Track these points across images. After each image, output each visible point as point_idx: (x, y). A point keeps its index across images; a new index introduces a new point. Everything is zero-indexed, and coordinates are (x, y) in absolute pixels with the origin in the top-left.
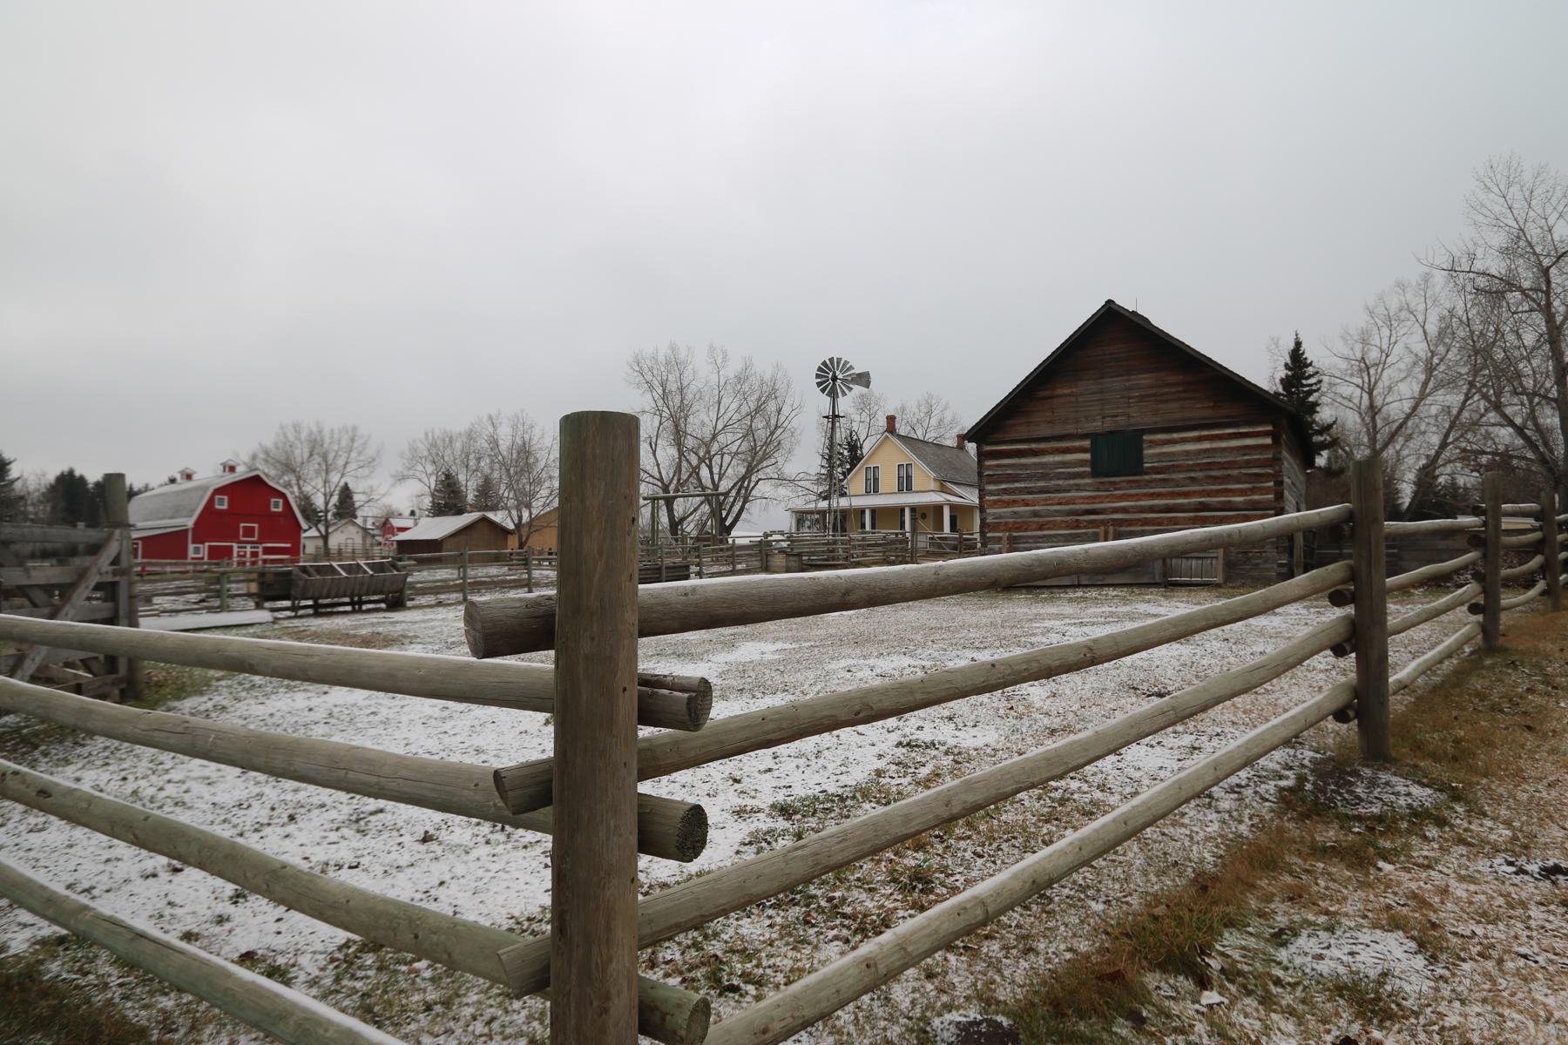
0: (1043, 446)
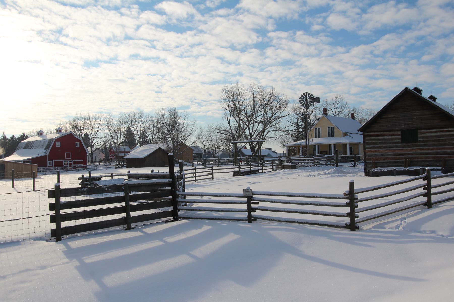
0: (385, 133)
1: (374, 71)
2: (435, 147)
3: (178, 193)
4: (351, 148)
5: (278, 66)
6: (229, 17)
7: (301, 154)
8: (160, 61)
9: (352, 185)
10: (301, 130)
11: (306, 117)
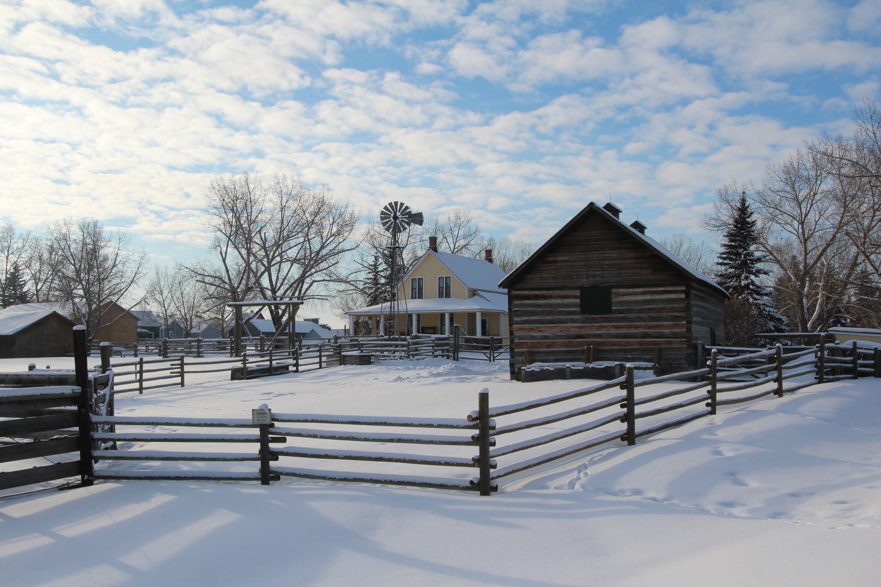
0: (550, 292)
1: (536, 167)
2: (643, 323)
3: (94, 418)
4: (484, 322)
5: (343, 142)
6: (240, 27)
7: (382, 333)
8: (69, 110)
9: (484, 398)
10: (383, 281)
11: (393, 253)
